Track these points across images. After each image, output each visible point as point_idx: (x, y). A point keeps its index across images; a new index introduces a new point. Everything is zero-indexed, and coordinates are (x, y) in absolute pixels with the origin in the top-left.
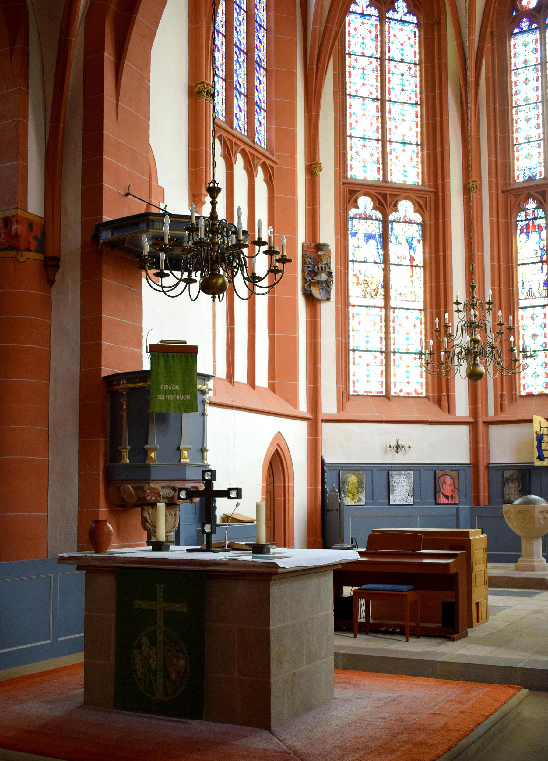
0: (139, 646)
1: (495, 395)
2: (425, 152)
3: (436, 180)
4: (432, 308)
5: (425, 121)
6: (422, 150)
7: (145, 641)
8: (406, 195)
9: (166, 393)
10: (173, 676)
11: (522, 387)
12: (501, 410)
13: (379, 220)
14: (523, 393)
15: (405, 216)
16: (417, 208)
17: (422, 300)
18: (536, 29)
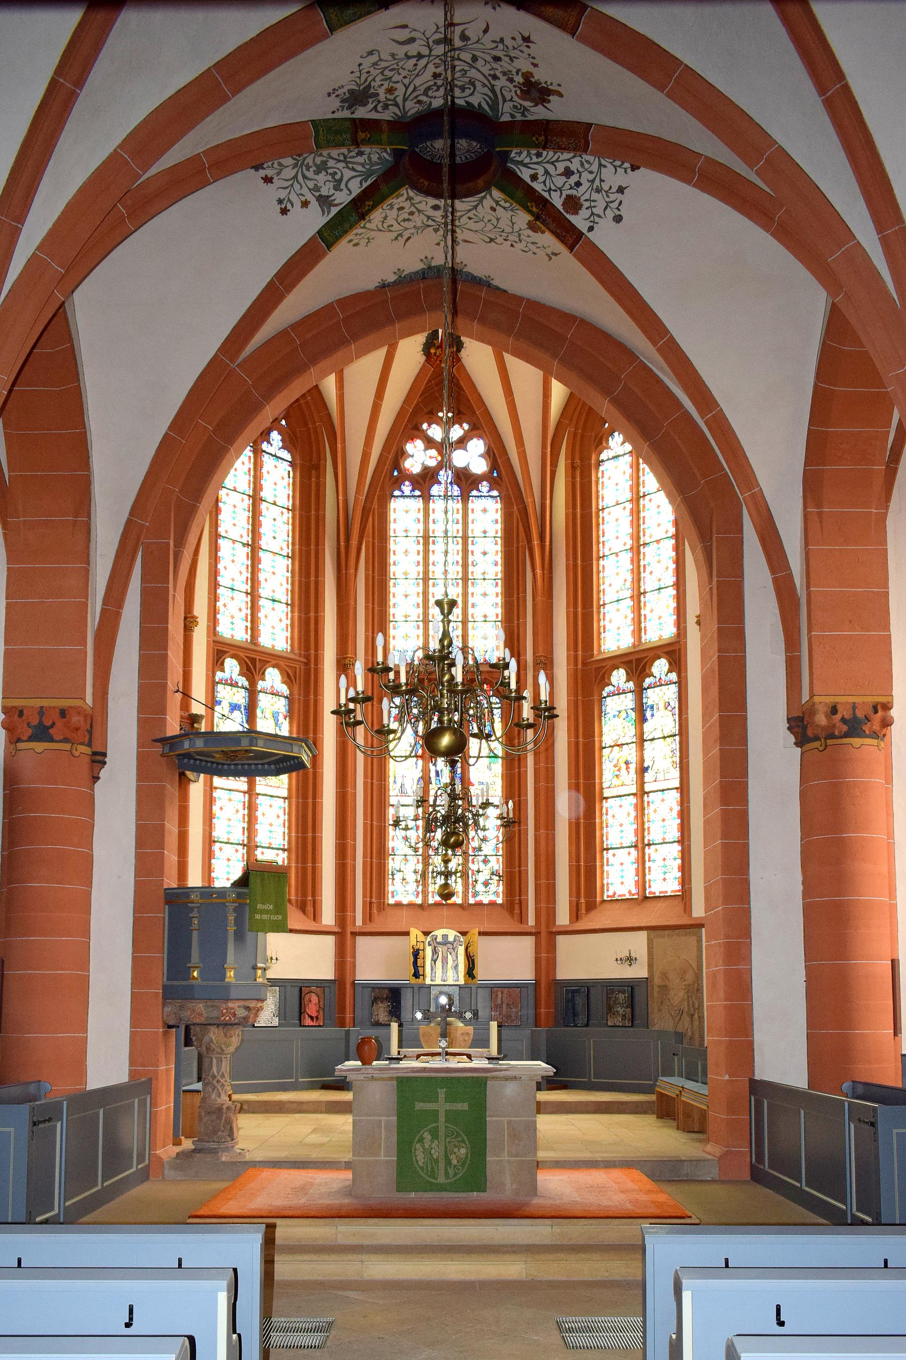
0: (421, 1140)
1: (364, 902)
2: (296, 614)
3: (307, 648)
4: (297, 797)
5: (297, 578)
6: (292, 612)
7: (427, 1136)
8: (276, 662)
9: (262, 912)
10: (455, 1162)
11: (390, 895)
12: (370, 920)
13: (246, 689)
14: (391, 901)
15: (272, 687)
16: (286, 679)
17: (287, 786)
18: (419, 496)
